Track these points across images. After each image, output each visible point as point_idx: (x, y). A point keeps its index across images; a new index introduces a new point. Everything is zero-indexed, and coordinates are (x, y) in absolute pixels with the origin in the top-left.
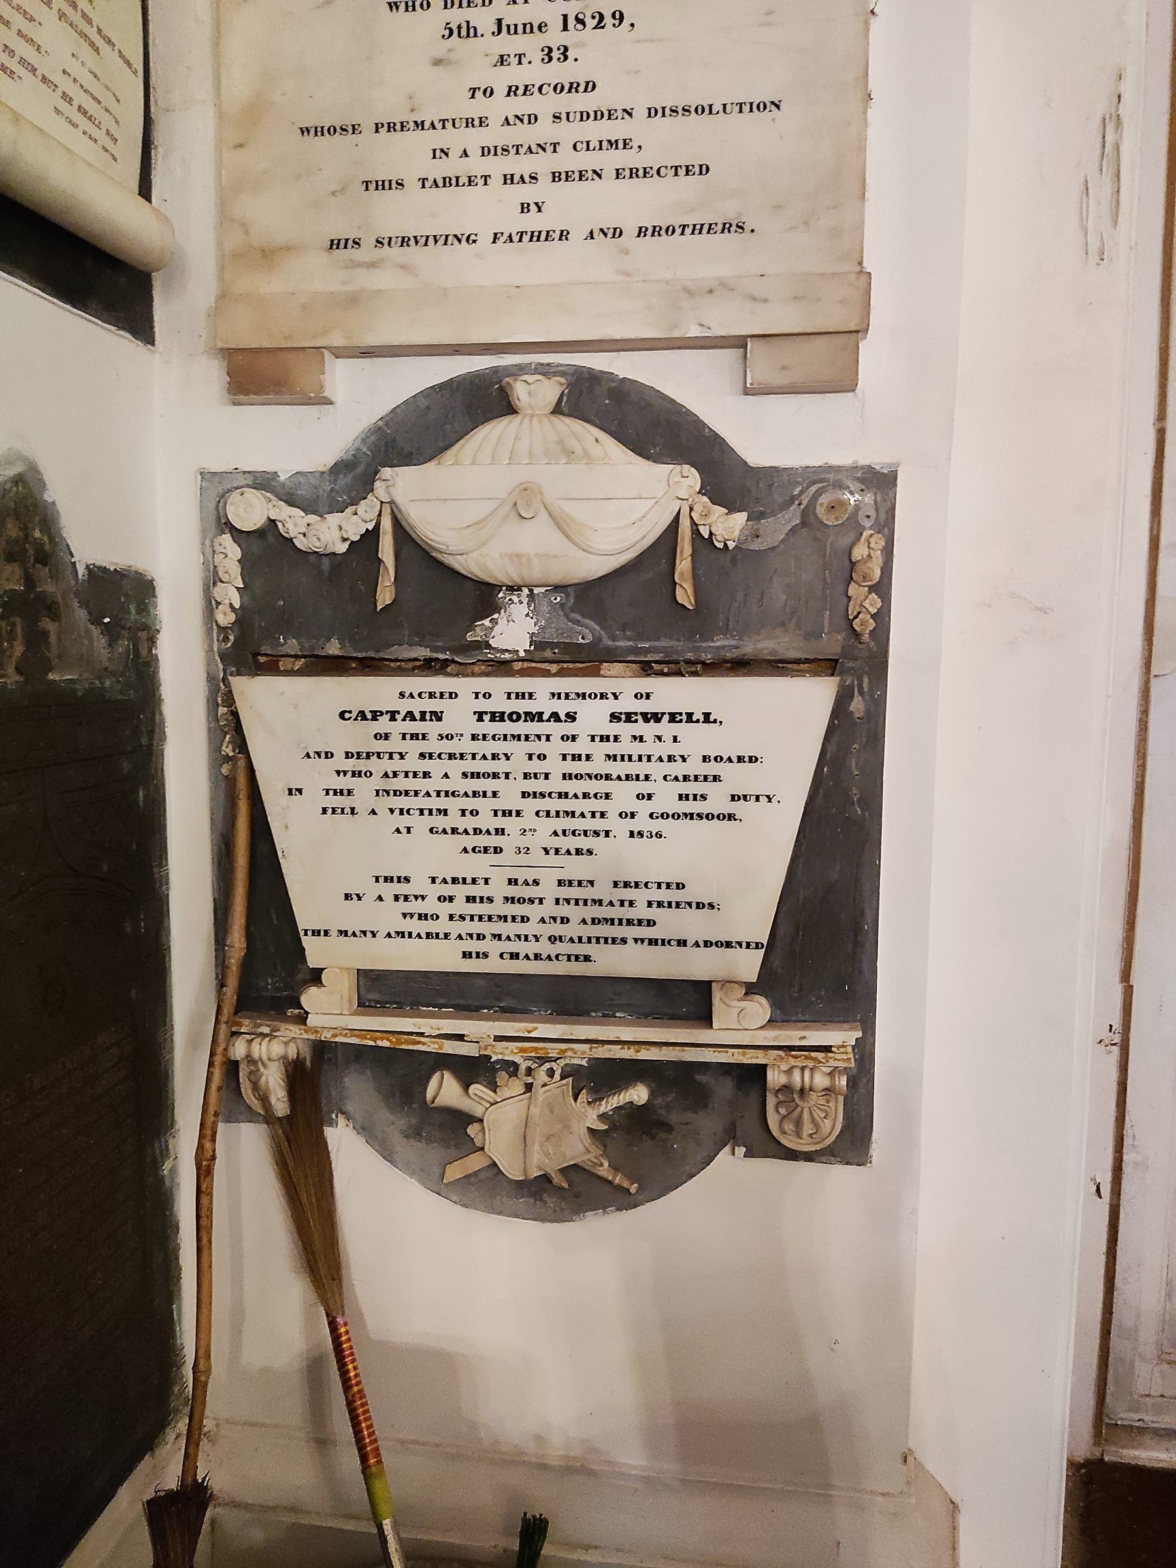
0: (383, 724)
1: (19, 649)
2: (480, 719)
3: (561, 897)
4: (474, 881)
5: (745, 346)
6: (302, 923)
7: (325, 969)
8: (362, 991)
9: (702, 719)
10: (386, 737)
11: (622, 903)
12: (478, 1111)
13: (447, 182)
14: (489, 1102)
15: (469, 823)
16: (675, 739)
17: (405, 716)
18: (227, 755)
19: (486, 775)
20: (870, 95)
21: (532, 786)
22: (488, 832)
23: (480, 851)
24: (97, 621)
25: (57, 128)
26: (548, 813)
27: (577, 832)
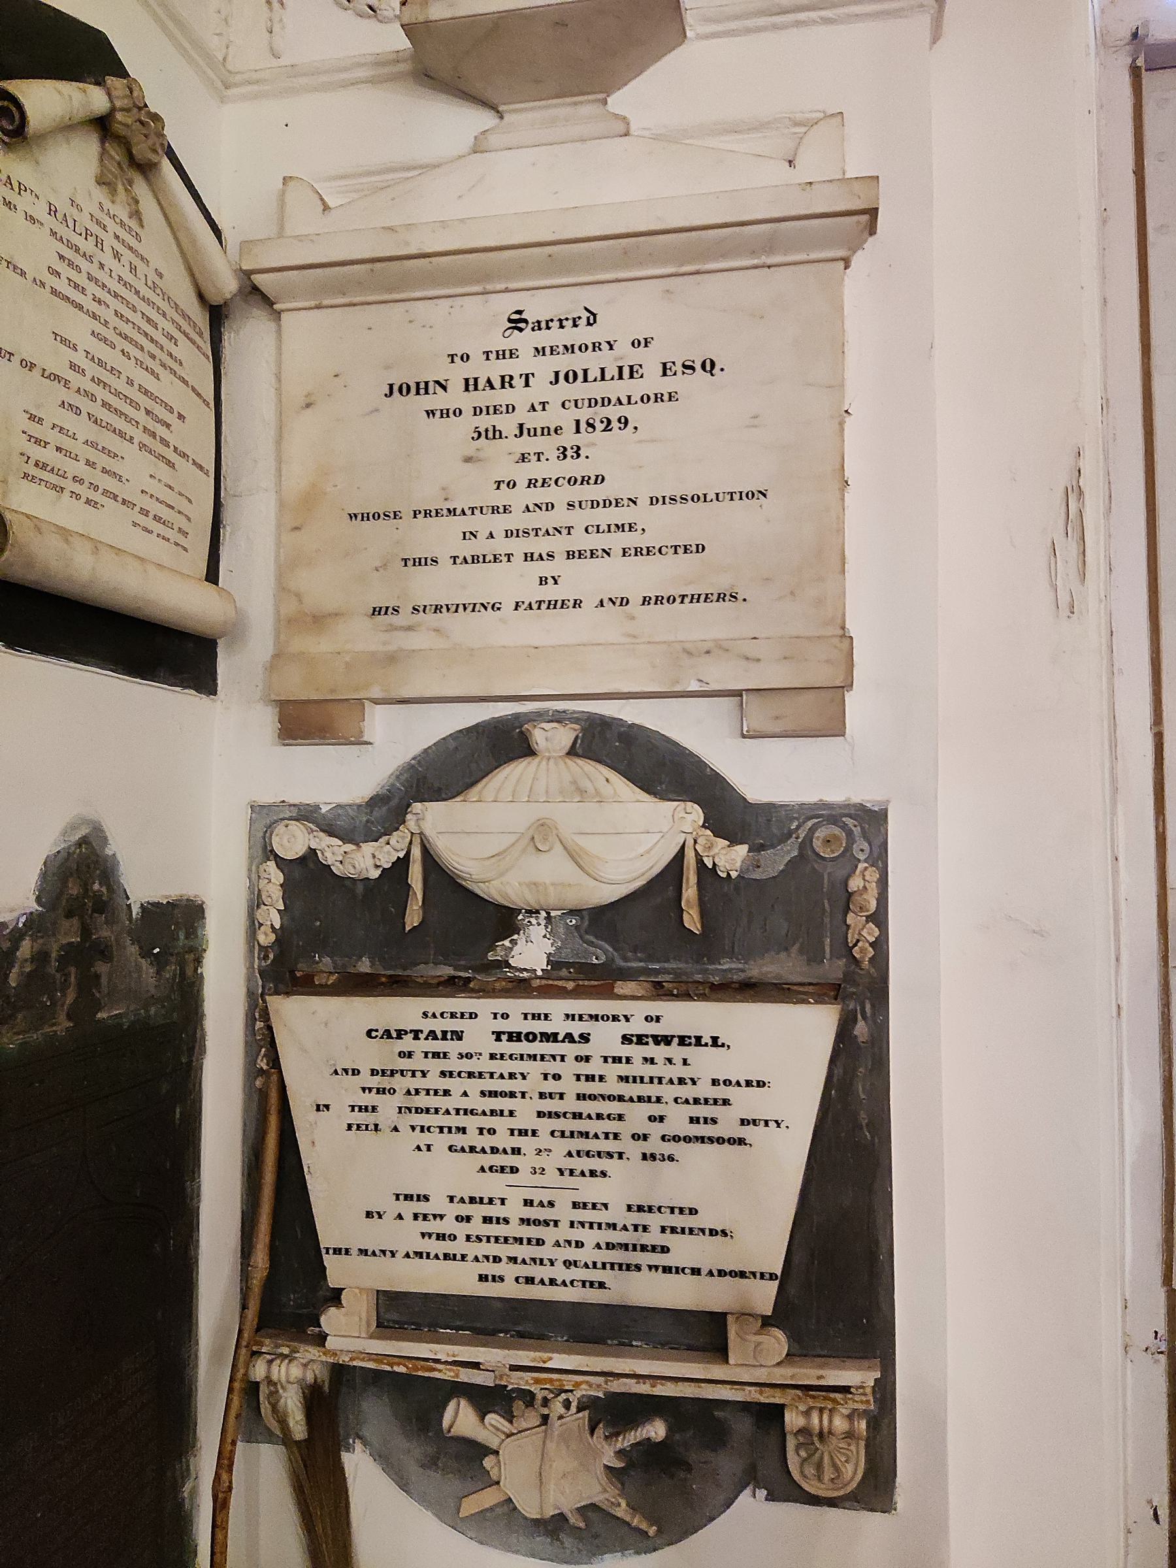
0: (407, 1043)
2: (498, 1039)
3: (576, 1219)
4: (491, 1201)
5: (741, 696)
6: (325, 1241)
7: (344, 1289)
8: (382, 1310)
9: (710, 1043)
10: (410, 1055)
11: (636, 1228)
12: (493, 1442)
13: (475, 559)
14: (504, 1433)
15: (487, 1141)
16: (685, 1062)
17: (428, 1035)
18: (262, 1068)
19: (503, 1094)
20: (846, 482)
21: (548, 1105)
22: (505, 1151)
23: (497, 1171)
24: (146, 953)
25: (137, 542)
26: (563, 1133)
27: (592, 1153)
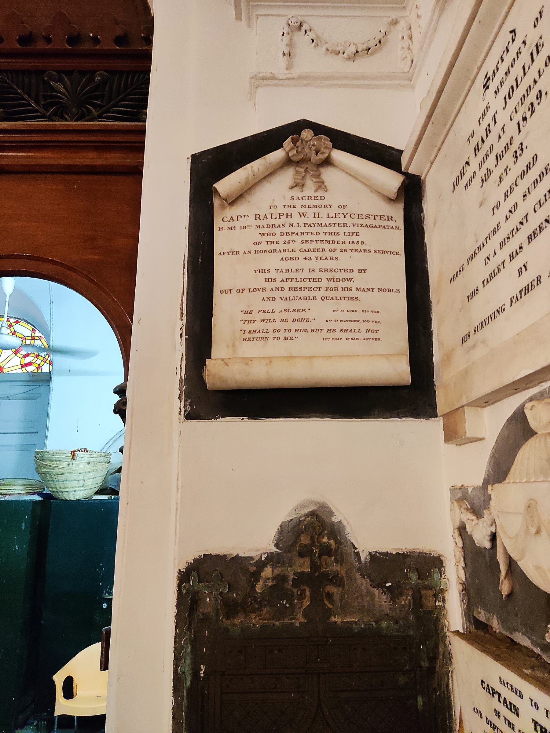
1: (306, 603)
